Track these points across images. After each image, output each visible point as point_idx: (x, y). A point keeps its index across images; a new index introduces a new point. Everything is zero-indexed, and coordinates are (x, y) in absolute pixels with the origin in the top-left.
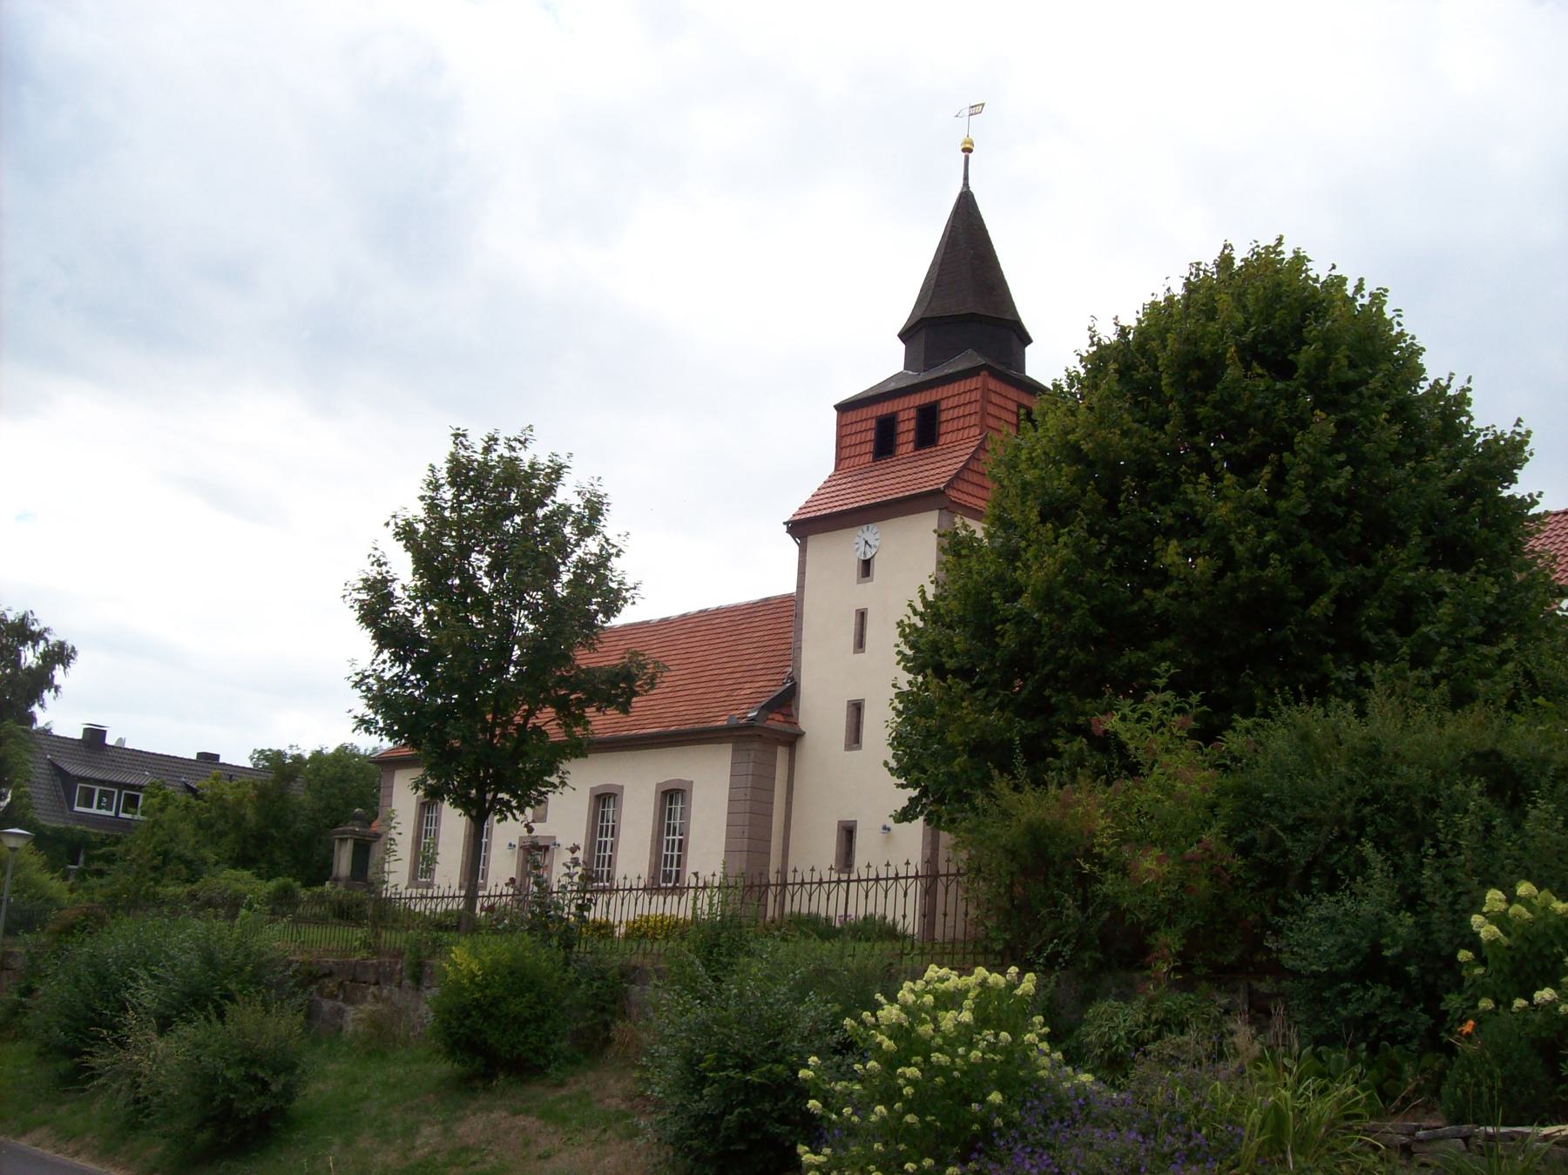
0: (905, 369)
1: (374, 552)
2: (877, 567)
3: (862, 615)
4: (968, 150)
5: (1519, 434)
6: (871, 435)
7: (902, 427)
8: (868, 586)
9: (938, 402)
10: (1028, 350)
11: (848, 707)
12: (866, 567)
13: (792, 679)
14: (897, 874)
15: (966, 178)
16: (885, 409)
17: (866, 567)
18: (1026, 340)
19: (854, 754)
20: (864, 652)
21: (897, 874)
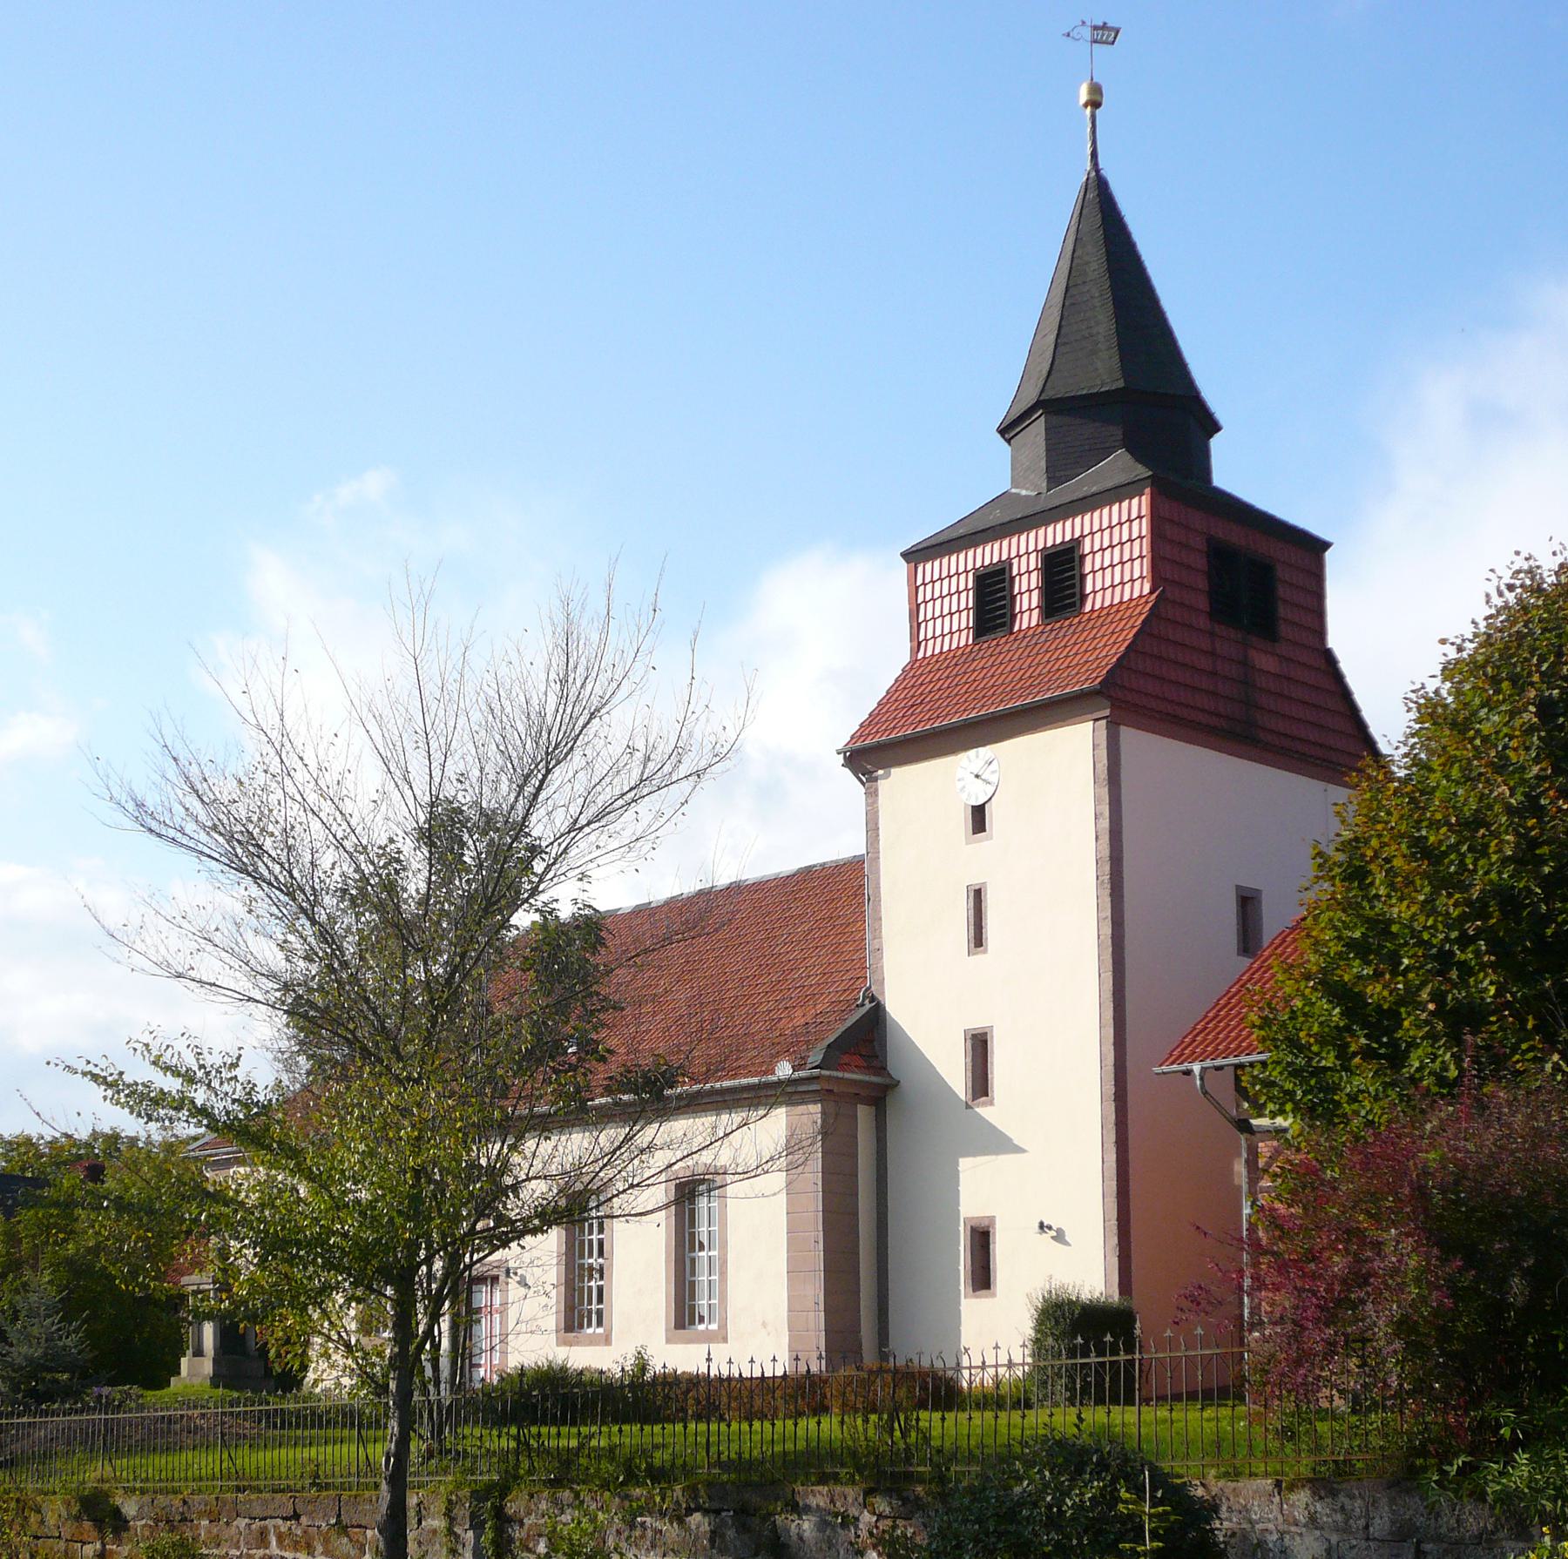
0: (1015, 483)
1: (205, 1052)
2: (993, 816)
3: (978, 895)
4: (1095, 104)
5: (1294, 1054)
6: (968, 599)
7: (1022, 584)
8: (983, 844)
9: (1077, 543)
10: (1216, 443)
11: (977, 1297)
12: (979, 819)
13: (873, 999)
14: (984, 1363)
15: (1094, 155)
16: (988, 555)
17: (979, 819)
18: (1215, 427)
19: (979, 958)
20: (985, 951)
21: (984, 1363)
